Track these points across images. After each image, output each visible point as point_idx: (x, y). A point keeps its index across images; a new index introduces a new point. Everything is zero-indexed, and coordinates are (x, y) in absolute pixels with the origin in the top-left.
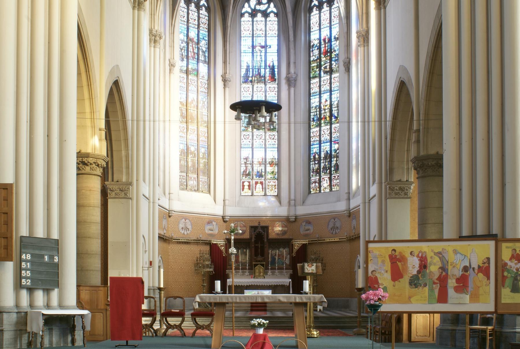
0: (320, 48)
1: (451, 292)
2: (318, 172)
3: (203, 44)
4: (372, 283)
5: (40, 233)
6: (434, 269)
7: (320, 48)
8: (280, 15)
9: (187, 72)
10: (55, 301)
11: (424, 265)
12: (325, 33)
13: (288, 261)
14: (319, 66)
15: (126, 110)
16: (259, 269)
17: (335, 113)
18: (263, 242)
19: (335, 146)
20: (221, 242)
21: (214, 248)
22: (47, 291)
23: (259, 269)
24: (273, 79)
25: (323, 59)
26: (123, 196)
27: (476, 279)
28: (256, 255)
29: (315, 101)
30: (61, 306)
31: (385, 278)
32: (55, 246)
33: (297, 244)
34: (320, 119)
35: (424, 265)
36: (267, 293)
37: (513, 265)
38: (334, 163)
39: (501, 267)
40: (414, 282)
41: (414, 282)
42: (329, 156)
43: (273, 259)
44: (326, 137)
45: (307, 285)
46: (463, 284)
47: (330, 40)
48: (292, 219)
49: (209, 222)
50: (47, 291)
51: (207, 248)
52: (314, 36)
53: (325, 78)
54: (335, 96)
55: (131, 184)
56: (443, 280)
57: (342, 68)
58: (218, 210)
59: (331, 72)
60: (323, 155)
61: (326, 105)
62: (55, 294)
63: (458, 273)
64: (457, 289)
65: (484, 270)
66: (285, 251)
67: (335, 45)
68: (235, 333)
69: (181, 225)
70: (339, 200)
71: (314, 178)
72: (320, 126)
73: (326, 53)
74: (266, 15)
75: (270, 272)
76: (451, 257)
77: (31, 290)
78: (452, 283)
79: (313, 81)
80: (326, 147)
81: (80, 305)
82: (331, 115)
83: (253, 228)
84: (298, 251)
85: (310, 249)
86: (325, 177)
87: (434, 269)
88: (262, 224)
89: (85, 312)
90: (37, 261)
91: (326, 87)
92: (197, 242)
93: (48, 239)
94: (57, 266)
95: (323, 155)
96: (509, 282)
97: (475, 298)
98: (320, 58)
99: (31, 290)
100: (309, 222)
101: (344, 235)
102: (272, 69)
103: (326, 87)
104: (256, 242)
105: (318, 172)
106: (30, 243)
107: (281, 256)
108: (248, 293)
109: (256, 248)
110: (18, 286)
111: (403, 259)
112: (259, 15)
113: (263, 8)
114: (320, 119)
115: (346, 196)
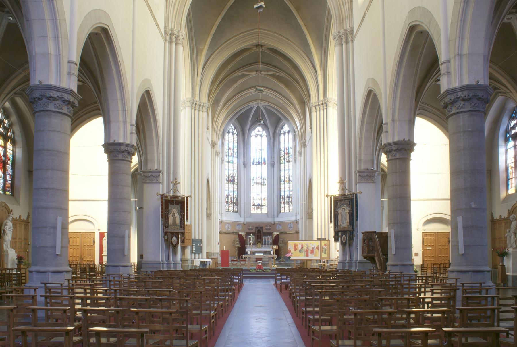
0: (284, 151)
1: (309, 254)
2: (284, 203)
3: (235, 150)
4: (289, 252)
5: (197, 238)
6: (305, 248)
7: (284, 151)
8: (268, 136)
9: (229, 162)
10: (201, 257)
11: (302, 247)
12: (287, 146)
13: (271, 241)
14: (284, 159)
15: (123, 78)
16: (259, 245)
17: (291, 179)
18: (261, 234)
19: (291, 193)
20: (243, 234)
21: (240, 236)
22: (199, 254)
23: (259, 245)
24: (265, 163)
25: (286, 156)
26: (155, 181)
27: (316, 251)
28: (258, 239)
29: (282, 174)
30: (202, 258)
31: (292, 250)
32: (200, 241)
33: (275, 234)
34: (284, 181)
35: (302, 247)
36: (262, 254)
37: (325, 247)
38: (290, 200)
39: (322, 247)
40: (300, 251)
41: (300, 251)
42: (288, 197)
43: (265, 240)
44: (287, 189)
45: (48, 305)
46: (312, 251)
47: (289, 149)
48: (273, 223)
49: (238, 225)
50: (199, 254)
51: (237, 236)
52: (282, 148)
53: (287, 164)
54: (291, 172)
55: (211, 214)
56: (307, 251)
57: (294, 161)
58: (242, 220)
59: (289, 161)
60: (286, 197)
61: (287, 176)
62: (201, 255)
63: (311, 249)
64: (311, 253)
65: (318, 248)
66: (270, 237)
67: (291, 151)
68: (189, 341)
69: (226, 226)
70: (292, 216)
71: (282, 206)
72: (284, 184)
73: (287, 153)
74: (261, 136)
75: (263, 246)
76: (309, 245)
77: (195, 254)
78: (310, 252)
79: (281, 165)
80: (287, 194)
81: (207, 258)
82: (289, 180)
83: (257, 228)
84: (275, 237)
85: (281, 236)
86: (287, 206)
87: (305, 248)
88: (260, 226)
89: (210, 260)
90: (196, 245)
91: (287, 168)
92: (233, 233)
93: (198, 239)
94: (201, 247)
95: (286, 197)
96: (324, 251)
97: (315, 255)
98: (284, 156)
99: (195, 254)
100: (280, 225)
101: (295, 230)
102: (264, 159)
103: (287, 168)
104: (258, 233)
105: (284, 203)
106: (194, 241)
107: (268, 239)
108: (256, 254)
109: (258, 236)
110: (192, 252)
111: (297, 245)
112: (259, 136)
113: (260, 133)
114: (284, 181)
115: (295, 214)
